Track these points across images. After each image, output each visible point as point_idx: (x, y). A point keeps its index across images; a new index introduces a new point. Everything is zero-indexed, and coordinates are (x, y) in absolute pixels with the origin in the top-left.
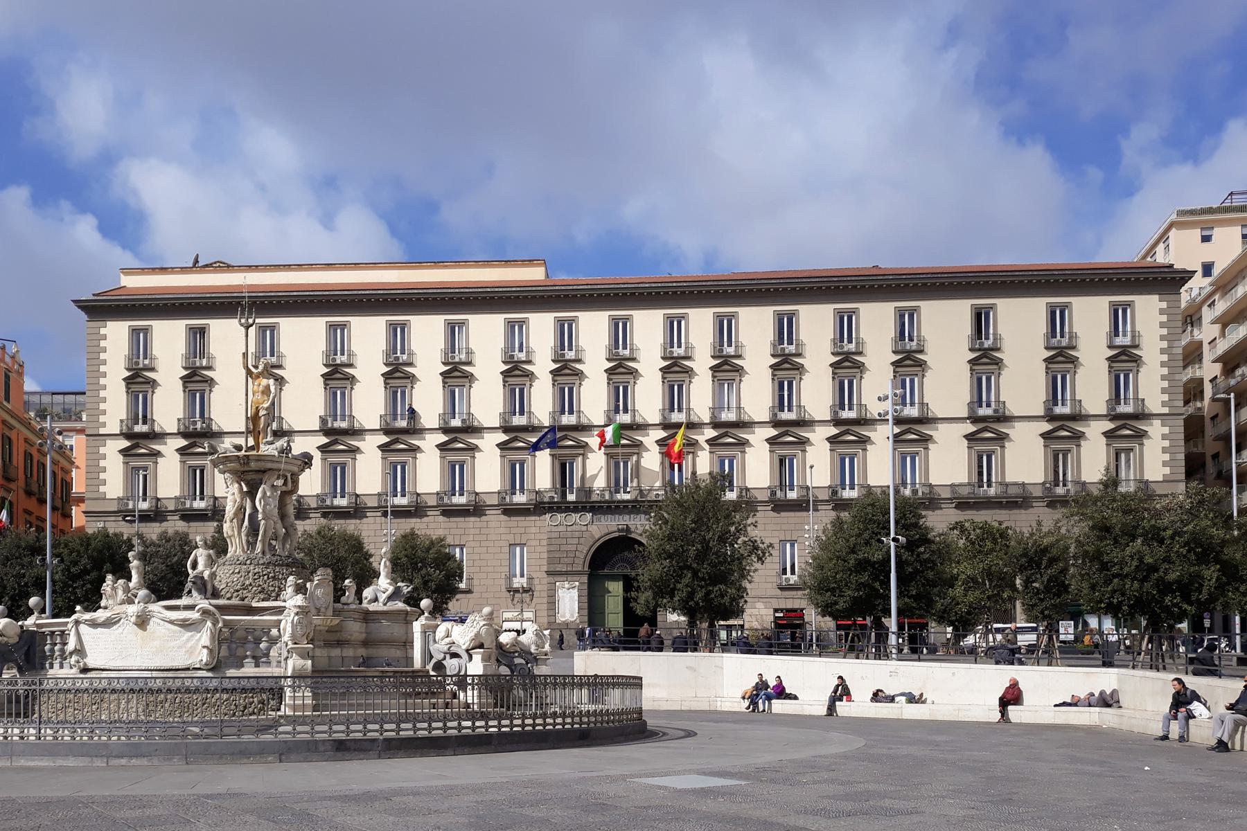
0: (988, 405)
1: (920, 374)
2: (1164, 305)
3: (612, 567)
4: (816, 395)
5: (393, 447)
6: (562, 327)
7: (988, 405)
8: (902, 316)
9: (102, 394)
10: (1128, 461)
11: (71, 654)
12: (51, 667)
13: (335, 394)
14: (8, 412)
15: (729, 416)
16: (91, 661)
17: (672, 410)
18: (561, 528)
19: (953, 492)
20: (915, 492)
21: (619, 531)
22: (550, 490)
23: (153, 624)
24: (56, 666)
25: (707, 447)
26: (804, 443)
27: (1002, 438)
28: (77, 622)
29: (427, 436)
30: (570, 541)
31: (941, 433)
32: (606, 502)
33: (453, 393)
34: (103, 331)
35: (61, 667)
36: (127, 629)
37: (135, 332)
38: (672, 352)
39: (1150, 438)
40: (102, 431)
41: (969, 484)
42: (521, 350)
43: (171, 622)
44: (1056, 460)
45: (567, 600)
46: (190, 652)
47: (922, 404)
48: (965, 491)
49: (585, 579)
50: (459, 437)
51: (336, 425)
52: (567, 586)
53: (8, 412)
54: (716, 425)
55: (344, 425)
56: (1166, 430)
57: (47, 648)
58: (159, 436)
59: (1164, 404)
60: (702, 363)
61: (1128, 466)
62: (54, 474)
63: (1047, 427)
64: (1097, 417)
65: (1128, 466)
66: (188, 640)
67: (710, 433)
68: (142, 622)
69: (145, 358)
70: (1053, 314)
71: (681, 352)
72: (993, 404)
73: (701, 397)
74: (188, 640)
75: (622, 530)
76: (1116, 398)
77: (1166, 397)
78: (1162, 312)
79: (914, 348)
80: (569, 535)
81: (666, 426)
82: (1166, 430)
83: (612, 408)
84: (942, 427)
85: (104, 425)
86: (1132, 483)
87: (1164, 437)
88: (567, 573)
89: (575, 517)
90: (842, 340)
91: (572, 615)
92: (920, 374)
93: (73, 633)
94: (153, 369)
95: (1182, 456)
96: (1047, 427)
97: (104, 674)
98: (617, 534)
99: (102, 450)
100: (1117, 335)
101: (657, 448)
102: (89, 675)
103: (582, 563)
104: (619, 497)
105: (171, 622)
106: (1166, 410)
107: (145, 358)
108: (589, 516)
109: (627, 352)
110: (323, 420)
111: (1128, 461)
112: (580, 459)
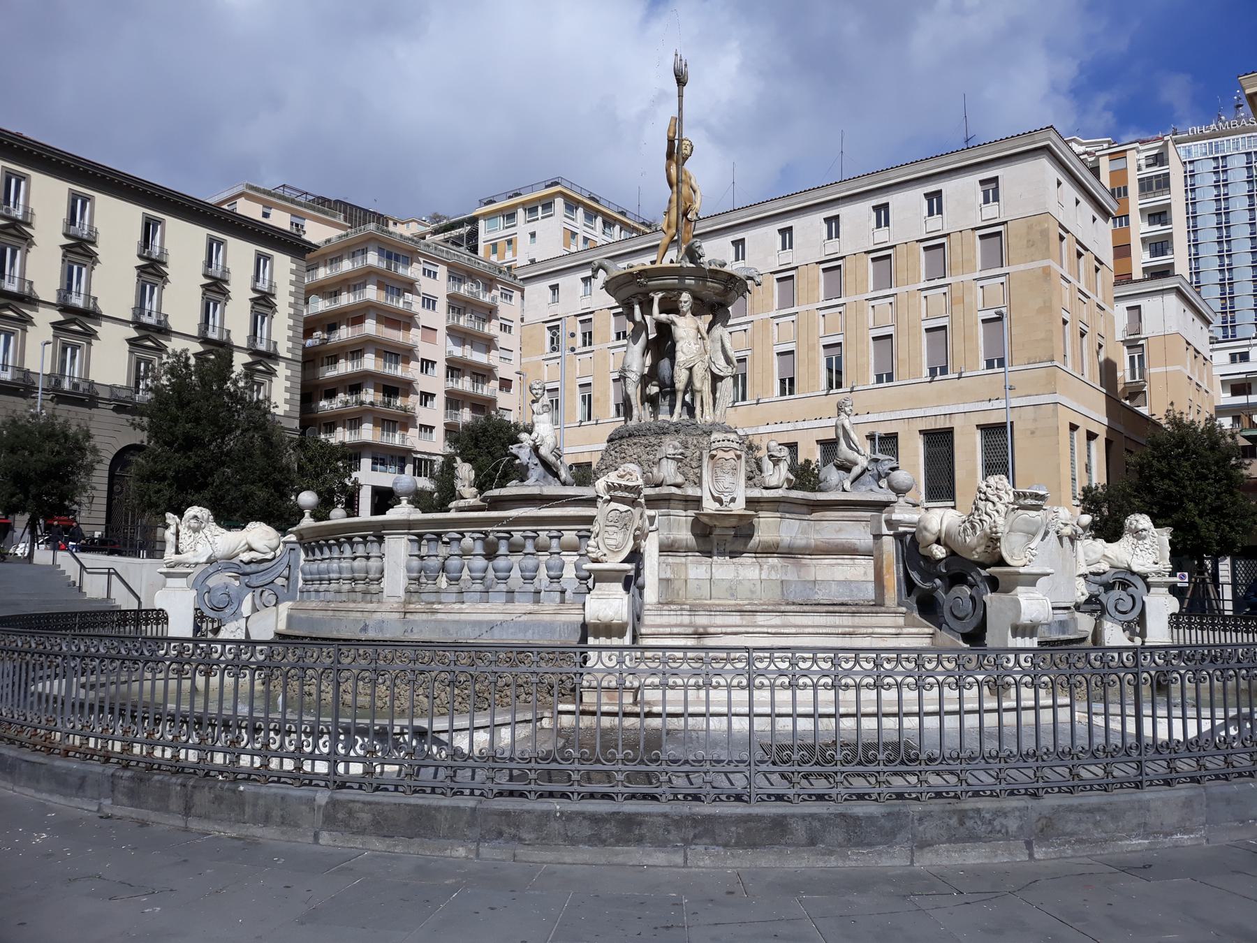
0: (150, 315)
1: (89, 265)
2: (294, 266)
5: (140, 342)
9: (291, 322)
10: (73, 357)
19: (112, 393)
20: (76, 386)
27: (90, 335)
29: (40, 309)
31: (104, 330)
39: (98, 339)
41: (128, 388)
48: (123, 394)
50: (78, 321)
56: (289, 373)
59: (289, 350)
61: (72, 363)
65: (72, 363)
72: (154, 314)
76: (67, 289)
77: (290, 345)
78: (292, 272)
81: (64, 308)
82: (289, 373)
84: (105, 324)
86: (1122, 552)
87: (287, 378)
95: (298, 397)
96: (59, 317)
106: (289, 356)
111: (73, 357)
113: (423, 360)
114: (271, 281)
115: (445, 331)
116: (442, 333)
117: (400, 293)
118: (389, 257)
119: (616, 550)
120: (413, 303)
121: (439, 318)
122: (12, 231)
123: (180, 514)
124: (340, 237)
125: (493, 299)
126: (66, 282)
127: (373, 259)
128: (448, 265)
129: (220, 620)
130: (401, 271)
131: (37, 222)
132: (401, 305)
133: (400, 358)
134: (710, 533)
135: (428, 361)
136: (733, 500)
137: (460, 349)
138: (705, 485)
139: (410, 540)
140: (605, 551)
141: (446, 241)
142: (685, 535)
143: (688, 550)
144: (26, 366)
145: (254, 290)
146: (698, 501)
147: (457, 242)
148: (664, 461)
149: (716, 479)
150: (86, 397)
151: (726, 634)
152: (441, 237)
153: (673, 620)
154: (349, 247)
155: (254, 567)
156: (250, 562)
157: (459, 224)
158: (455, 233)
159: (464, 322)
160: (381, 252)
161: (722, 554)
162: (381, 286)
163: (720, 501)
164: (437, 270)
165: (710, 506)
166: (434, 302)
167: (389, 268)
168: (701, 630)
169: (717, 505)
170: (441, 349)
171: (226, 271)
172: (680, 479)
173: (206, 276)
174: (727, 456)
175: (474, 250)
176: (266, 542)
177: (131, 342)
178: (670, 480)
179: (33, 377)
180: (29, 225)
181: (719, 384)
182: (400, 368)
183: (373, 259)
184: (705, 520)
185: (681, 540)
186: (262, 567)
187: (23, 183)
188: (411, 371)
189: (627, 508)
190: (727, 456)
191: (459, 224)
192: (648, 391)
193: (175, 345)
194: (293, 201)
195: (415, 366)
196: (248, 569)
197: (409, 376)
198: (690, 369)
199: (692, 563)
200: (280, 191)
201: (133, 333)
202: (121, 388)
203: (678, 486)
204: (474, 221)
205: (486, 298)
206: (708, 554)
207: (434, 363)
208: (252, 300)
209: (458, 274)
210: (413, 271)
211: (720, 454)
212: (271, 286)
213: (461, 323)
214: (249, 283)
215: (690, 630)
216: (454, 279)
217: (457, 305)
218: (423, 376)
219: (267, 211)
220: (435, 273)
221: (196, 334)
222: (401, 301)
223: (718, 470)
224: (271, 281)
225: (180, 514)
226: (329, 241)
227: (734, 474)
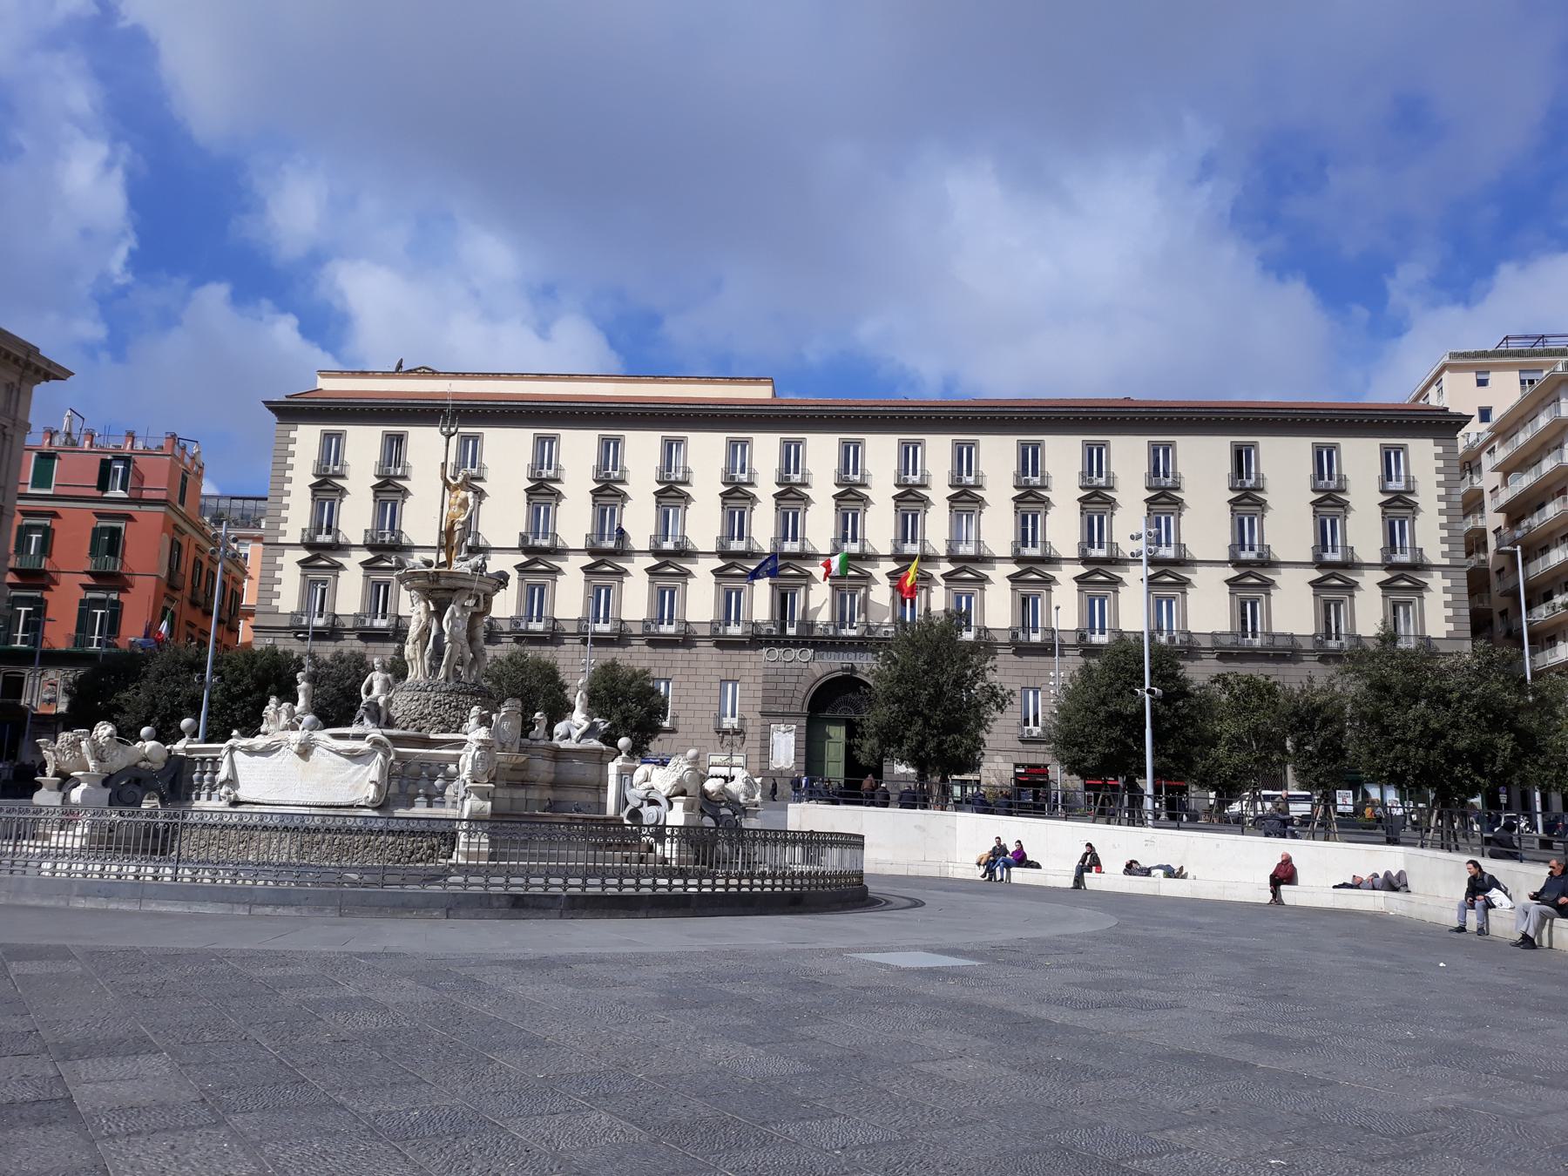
0: (1252, 549)
7: (1252, 549)
8: (1156, 451)
10: (1407, 615)
11: (222, 784)
12: (198, 798)
13: (538, 510)
14: (181, 515)
15: (967, 550)
16: (243, 794)
17: (905, 540)
19: (1214, 641)
20: (1171, 639)
22: (768, 623)
23: (316, 755)
24: (204, 797)
25: (943, 582)
28: (232, 749)
31: (1282, 578)
32: (830, 637)
34: (292, 435)
35: (209, 798)
36: (287, 759)
37: (327, 436)
40: (281, 540)
43: (338, 752)
46: (356, 788)
47: (1179, 545)
48: (1227, 641)
51: (537, 543)
53: (181, 515)
54: (952, 558)
55: (546, 543)
57: (195, 776)
58: (691, 555)
59: (1444, 555)
60: (939, 492)
62: (224, 583)
63: (1316, 574)
66: (355, 774)
67: (947, 567)
68: (305, 751)
69: (336, 464)
70: (1320, 455)
71: (917, 479)
73: (936, 528)
74: (355, 774)
75: (846, 669)
76: (1391, 546)
78: (1437, 457)
80: (787, 672)
83: (780, 535)
85: (284, 533)
88: (783, 715)
89: (795, 653)
90: (1091, 474)
93: (226, 760)
94: (343, 477)
97: (257, 809)
98: (840, 674)
99: (279, 560)
100: (1390, 479)
102: (239, 809)
103: (800, 704)
104: (844, 632)
105: (338, 752)
106: (1446, 562)
107: (336, 464)
108: (810, 652)
110: (523, 537)
111: (1407, 615)
112: (803, 590)
126: (781, 528)
131: (694, 479)
144: (1274, 630)
150: (554, 637)
171: (1342, 479)
173: (1383, 492)
177: (1231, 582)
179: (1300, 641)
180: (1261, 490)
193: (417, 559)
194: (1519, 354)
200: (1503, 348)
201: (1232, 573)
202: (1222, 634)
219: (1481, 377)
224: (1407, 476)
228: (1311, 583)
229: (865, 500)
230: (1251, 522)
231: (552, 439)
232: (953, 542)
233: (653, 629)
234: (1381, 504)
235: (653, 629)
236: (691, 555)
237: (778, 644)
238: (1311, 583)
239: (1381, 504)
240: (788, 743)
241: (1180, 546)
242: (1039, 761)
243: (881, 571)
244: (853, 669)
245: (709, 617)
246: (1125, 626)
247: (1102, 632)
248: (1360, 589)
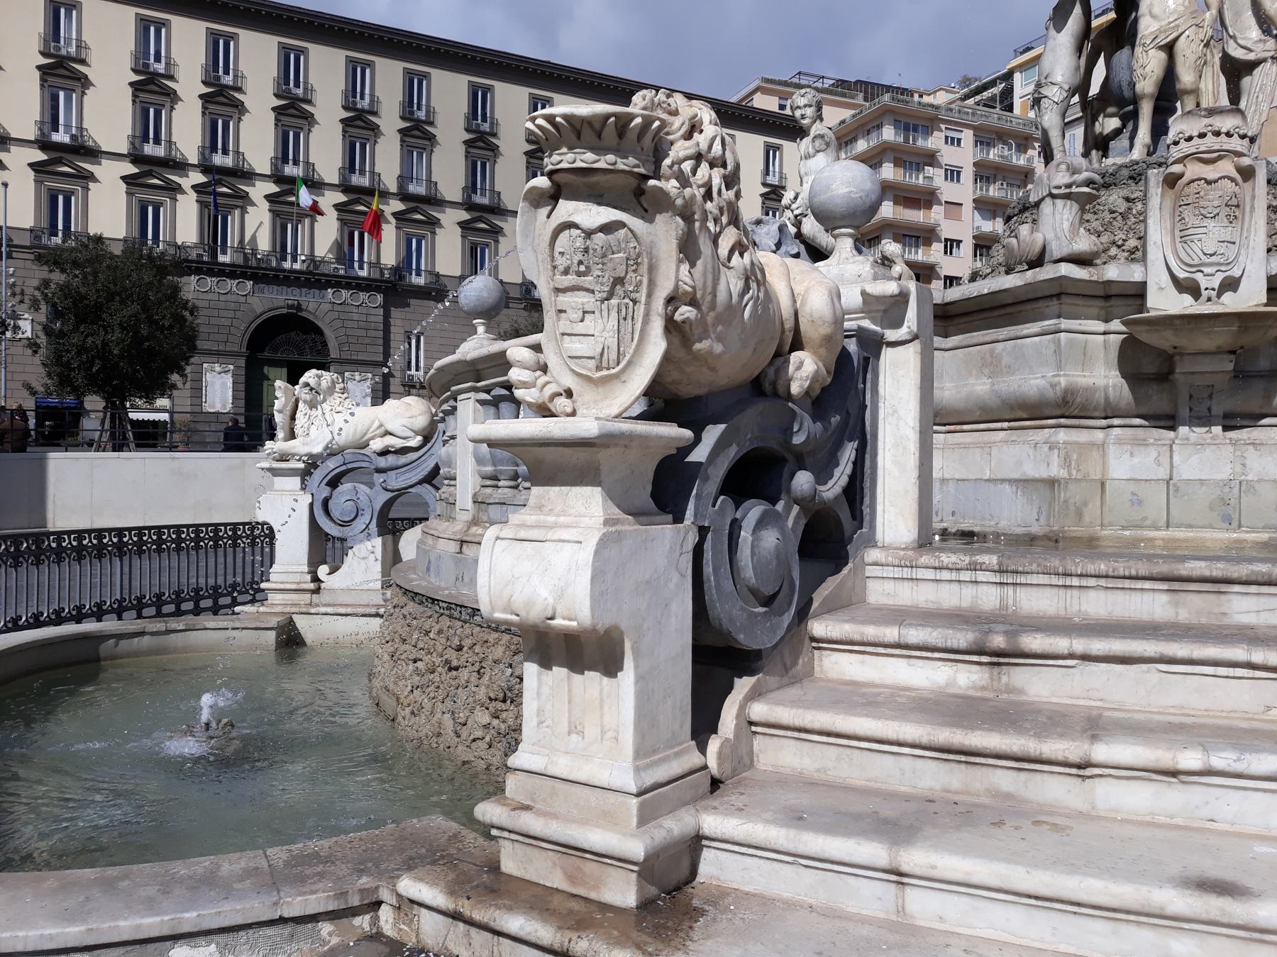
3: (275, 350)
4: (256, 141)
5: (50, 168)
6: (216, 44)
17: (285, 160)
18: (210, 296)
21: (289, 307)
22: (196, 246)
25: (393, 221)
26: (434, 224)
29: (13, 148)
30: (223, 313)
32: (272, 269)
33: (55, 99)
38: (354, 103)
42: (158, 59)
44: (142, 215)
45: (218, 386)
47: (307, 163)
49: (242, 362)
52: (358, 377)
54: (404, 196)
58: (439, 203)
60: (390, 121)
64: (453, 204)
67: (198, 178)
73: (386, 160)
75: (292, 307)
76: (471, 187)
79: (367, 107)
80: (222, 305)
83: (48, 118)
88: (219, 354)
89: (231, 284)
90: (216, 69)
91: (224, 406)
92: (168, 105)
96: (131, 169)
98: (285, 311)
101: (266, 205)
103: (238, 342)
104: (287, 265)
108: (249, 284)
109: (300, 92)
112: (237, 212)
113: (946, 240)
114: (781, 173)
115: (971, 205)
116: (968, 206)
117: (919, 168)
118: (906, 129)
119: (605, 371)
120: (936, 176)
121: (964, 191)
122: (292, 111)
123: (293, 380)
124: (854, 116)
125: (1029, 160)
127: (889, 133)
128: (974, 128)
129: (343, 540)
130: (920, 143)
132: (921, 181)
133: (921, 241)
134: (1171, 371)
135: (952, 241)
136: (1231, 284)
137: (991, 223)
138: (1154, 254)
139: (482, 403)
140: (569, 381)
141: (978, 104)
142: (1103, 377)
143: (1110, 412)
145: (764, 184)
146: (1137, 293)
147: (989, 104)
148: (1047, 207)
149: (1183, 236)
151: (1086, 658)
152: (971, 101)
153: (950, 596)
154: (863, 125)
155: (391, 460)
156: (384, 453)
157: (992, 83)
158: (986, 94)
159: (994, 191)
160: (896, 124)
161: (1203, 420)
162: (898, 163)
163: (1191, 288)
164: (961, 136)
165: (1165, 301)
166: (959, 173)
167: (906, 140)
168: (998, 641)
169: (1187, 299)
170: (966, 226)
171: (782, 177)
172: (1084, 244)
174: (1210, 172)
175: (1010, 108)
176: (405, 421)
178: (1056, 250)
180: (375, 114)
181: (1246, 81)
182: (920, 251)
183: (889, 133)
184: (1164, 340)
185: (1091, 390)
186: (403, 459)
187: (368, 71)
188: (934, 254)
189: (607, 214)
190: (1210, 172)
191: (992, 83)
192: (1098, 128)
195: (938, 247)
196: (382, 462)
197: (932, 260)
198: (1169, 48)
199: (1120, 442)
200: (796, 80)
203: (1081, 260)
204: (1008, 76)
205: (1020, 161)
206: (1168, 421)
207: (959, 242)
208: (762, 195)
209: (985, 137)
210: (935, 141)
211: (1193, 170)
212: (781, 178)
213: (991, 193)
214: (758, 178)
215: (962, 638)
216: (982, 143)
217: (985, 173)
218: (948, 258)
219: (783, 102)
220: (959, 140)
221: (125, 152)
222: (921, 177)
223: (1188, 213)
224: (781, 173)
225: (293, 380)
226: (843, 122)
227: (1232, 219)
228: (124, 178)
229: (309, 118)
230: (484, 165)
231: (160, 24)
232: (404, 179)
233: (44, 240)
234: (400, 131)
235: (44, 240)
236: (94, 154)
237: (211, 273)
238: (124, 178)
239: (342, 121)
240: (224, 385)
241: (431, 183)
242: (1201, 455)
243: (260, 191)
244: (299, 308)
245: (28, 222)
246: (441, 268)
247: (418, 274)
248: (441, 227)
